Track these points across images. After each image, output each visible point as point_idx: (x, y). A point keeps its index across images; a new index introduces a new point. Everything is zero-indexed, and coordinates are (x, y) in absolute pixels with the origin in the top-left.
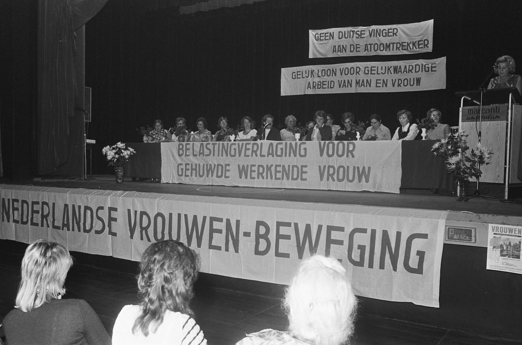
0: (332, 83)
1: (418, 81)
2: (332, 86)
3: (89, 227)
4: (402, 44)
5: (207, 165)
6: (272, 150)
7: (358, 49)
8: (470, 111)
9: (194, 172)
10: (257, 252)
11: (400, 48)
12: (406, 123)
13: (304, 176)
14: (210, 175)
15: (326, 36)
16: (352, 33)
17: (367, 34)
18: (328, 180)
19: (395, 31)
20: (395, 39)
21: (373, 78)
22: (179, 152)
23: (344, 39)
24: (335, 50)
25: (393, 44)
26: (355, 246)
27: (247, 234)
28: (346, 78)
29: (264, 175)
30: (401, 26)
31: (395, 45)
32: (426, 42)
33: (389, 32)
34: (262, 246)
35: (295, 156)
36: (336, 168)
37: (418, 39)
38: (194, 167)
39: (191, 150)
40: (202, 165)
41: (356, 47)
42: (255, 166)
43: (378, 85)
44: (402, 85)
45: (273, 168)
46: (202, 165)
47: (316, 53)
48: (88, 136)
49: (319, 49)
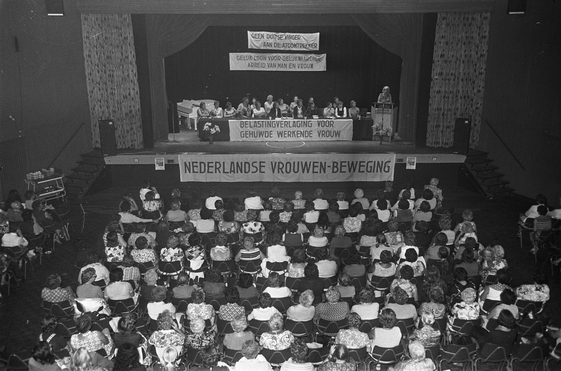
0: (264, 64)
1: (312, 65)
2: (264, 66)
4: (303, 45)
5: (259, 132)
6: (295, 124)
7: (279, 46)
9: (251, 135)
10: (333, 172)
11: (302, 47)
14: (261, 136)
15: (259, 36)
16: (275, 36)
17: (284, 37)
18: (322, 136)
19: (299, 37)
20: (299, 41)
21: (288, 63)
22: (241, 126)
23: (270, 39)
25: (298, 44)
26: (369, 167)
27: (329, 167)
28: (273, 62)
29: (291, 135)
30: (302, 34)
31: (299, 45)
32: (316, 45)
33: (296, 37)
34: (335, 169)
35: (306, 126)
36: (326, 131)
37: (312, 42)
38: (251, 133)
39: (249, 125)
40: (256, 132)
41: (278, 44)
42: (286, 131)
43: (290, 67)
44: (303, 67)
45: (296, 133)
46: (256, 132)
47: (253, 45)
49: (255, 43)
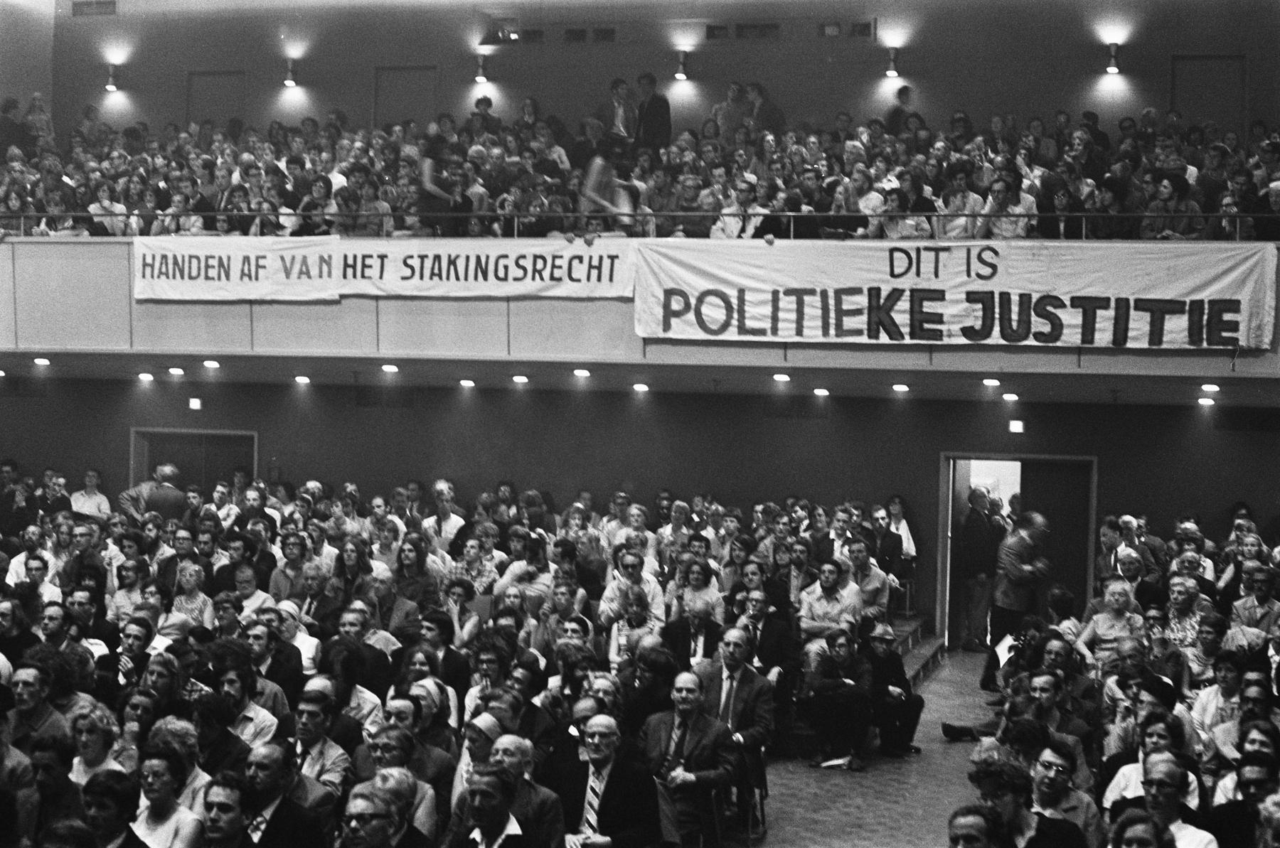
3: (1044, 324)
8: (788, 303)
12: (498, 519)
24: (436, 271)
48: (964, 450)
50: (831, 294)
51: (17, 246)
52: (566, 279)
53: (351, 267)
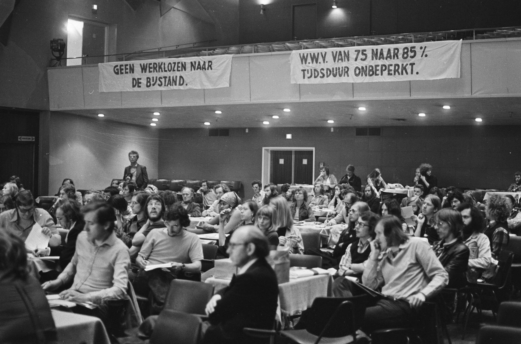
13: (140, 85)
50: (344, 68)
51: (83, 68)
52: (168, 71)
53: (314, 58)
